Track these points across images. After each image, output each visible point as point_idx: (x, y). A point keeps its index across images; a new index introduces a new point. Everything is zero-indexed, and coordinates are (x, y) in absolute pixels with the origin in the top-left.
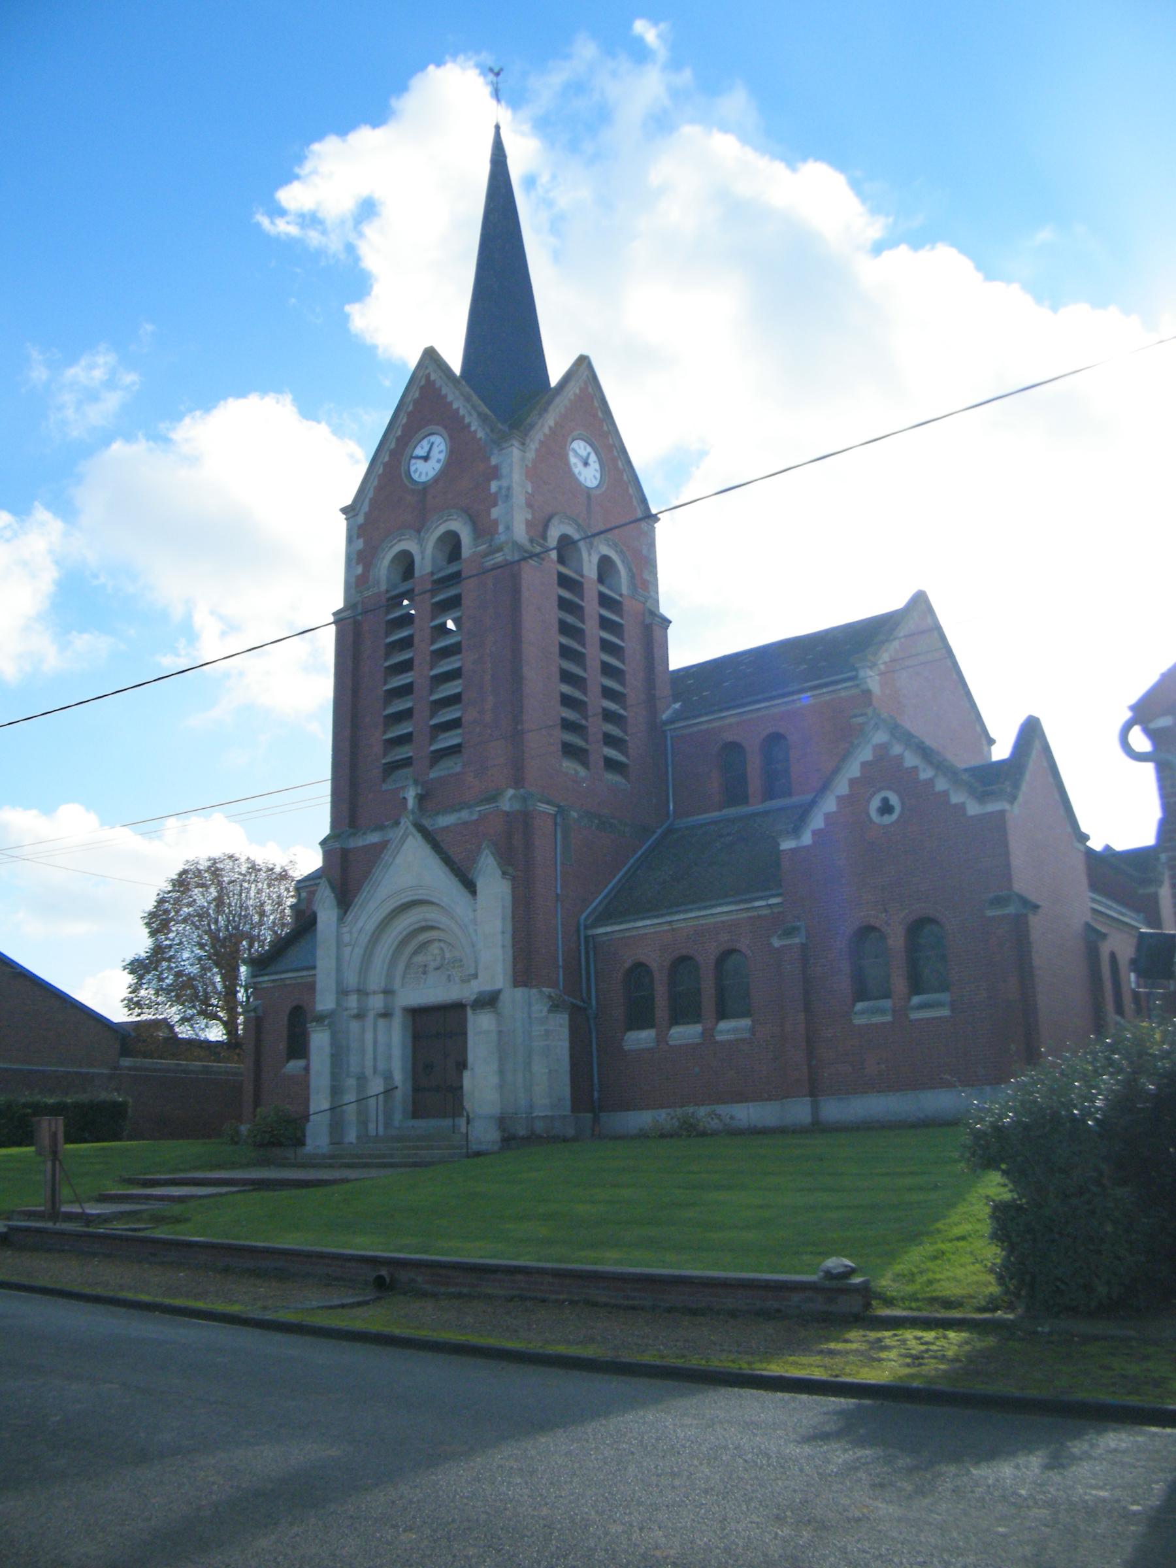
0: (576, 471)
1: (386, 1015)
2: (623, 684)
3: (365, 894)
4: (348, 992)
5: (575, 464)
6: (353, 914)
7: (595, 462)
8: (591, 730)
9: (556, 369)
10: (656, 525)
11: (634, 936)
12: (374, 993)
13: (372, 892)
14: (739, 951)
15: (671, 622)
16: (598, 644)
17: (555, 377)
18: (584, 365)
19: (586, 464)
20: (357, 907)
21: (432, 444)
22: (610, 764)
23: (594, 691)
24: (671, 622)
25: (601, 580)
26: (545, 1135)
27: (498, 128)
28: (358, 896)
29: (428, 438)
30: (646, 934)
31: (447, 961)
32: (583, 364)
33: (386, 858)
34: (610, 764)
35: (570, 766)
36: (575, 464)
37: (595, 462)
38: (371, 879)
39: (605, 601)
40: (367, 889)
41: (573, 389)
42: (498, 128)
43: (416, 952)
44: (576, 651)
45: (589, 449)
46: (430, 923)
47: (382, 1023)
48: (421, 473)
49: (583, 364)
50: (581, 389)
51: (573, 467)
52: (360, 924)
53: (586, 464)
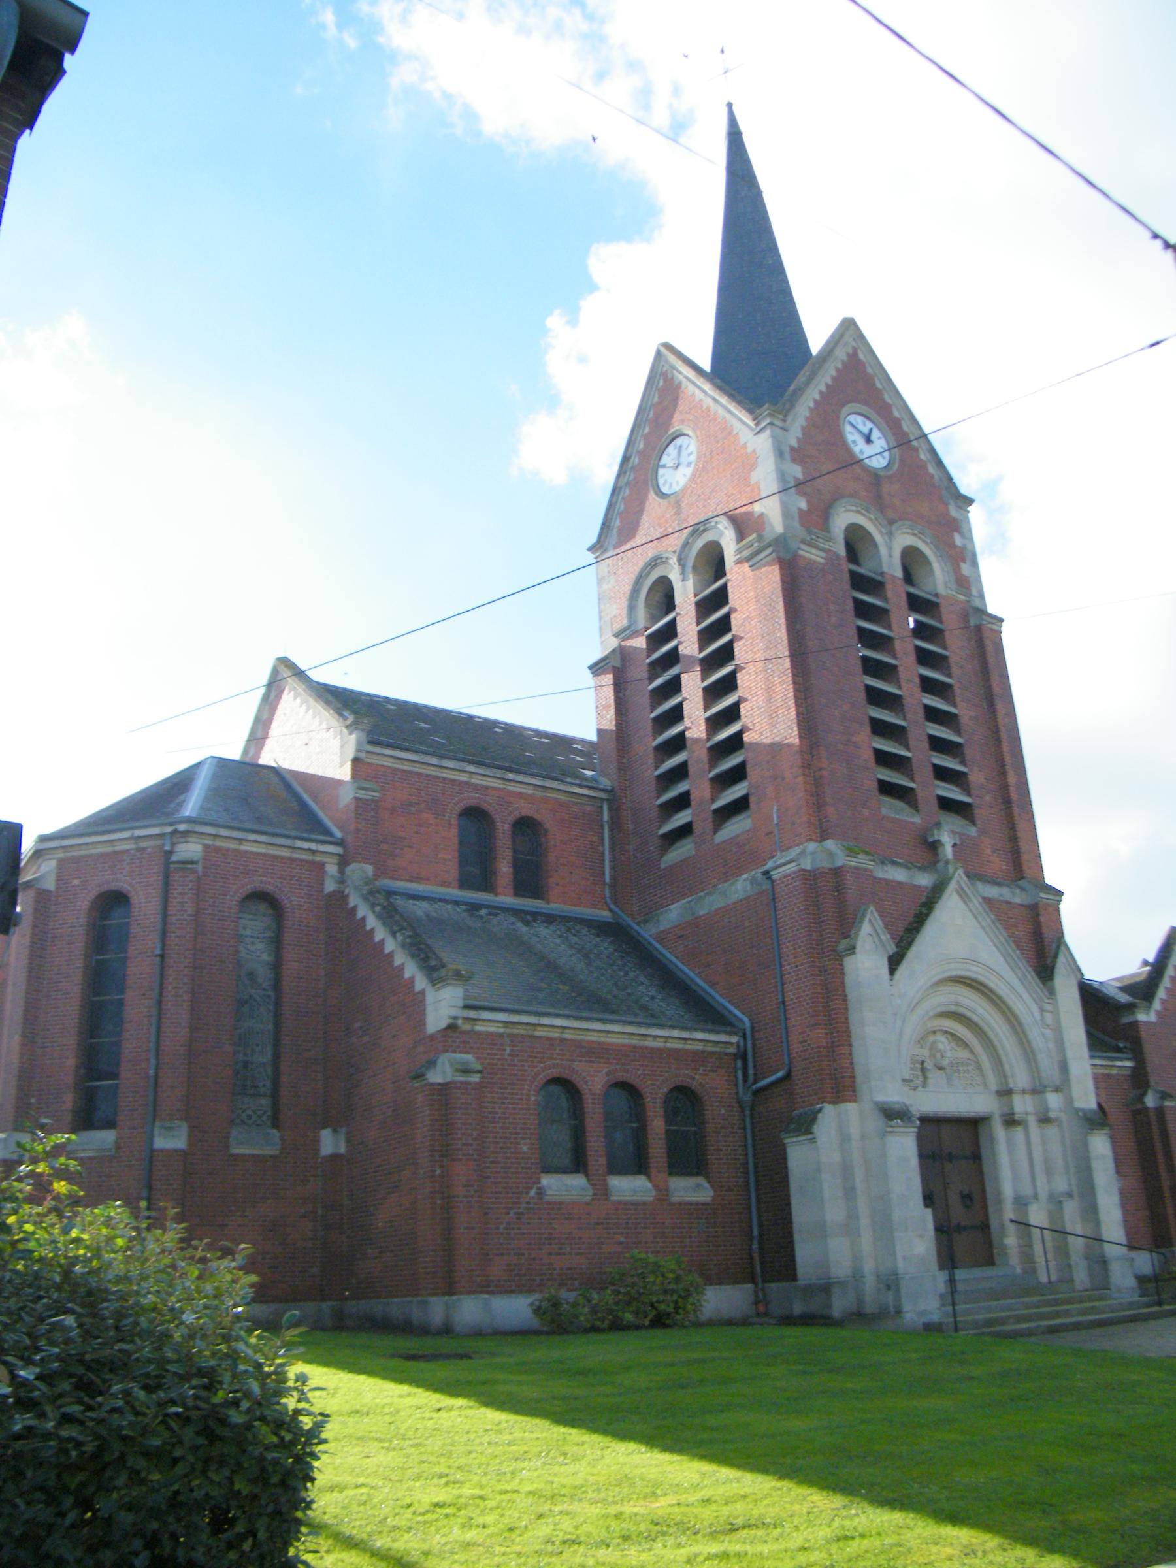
0: (856, 450)
2: (958, 732)
5: (854, 442)
7: (879, 438)
8: (920, 794)
9: (817, 337)
10: (969, 509)
15: (1002, 620)
16: (935, 802)
17: (816, 344)
18: (852, 327)
19: (868, 440)
21: (681, 447)
22: (946, 804)
23: (923, 773)
24: (1002, 620)
25: (908, 578)
27: (730, 105)
29: (673, 443)
32: (849, 327)
34: (946, 804)
35: (891, 808)
36: (854, 442)
37: (879, 438)
39: (916, 604)
41: (841, 354)
42: (730, 105)
44: (882, 635)
45: (869, 425)
48: (671, 485)
49: (849, 327)
50: (848, 354)
51: (852, 445)
53: (868, 440)
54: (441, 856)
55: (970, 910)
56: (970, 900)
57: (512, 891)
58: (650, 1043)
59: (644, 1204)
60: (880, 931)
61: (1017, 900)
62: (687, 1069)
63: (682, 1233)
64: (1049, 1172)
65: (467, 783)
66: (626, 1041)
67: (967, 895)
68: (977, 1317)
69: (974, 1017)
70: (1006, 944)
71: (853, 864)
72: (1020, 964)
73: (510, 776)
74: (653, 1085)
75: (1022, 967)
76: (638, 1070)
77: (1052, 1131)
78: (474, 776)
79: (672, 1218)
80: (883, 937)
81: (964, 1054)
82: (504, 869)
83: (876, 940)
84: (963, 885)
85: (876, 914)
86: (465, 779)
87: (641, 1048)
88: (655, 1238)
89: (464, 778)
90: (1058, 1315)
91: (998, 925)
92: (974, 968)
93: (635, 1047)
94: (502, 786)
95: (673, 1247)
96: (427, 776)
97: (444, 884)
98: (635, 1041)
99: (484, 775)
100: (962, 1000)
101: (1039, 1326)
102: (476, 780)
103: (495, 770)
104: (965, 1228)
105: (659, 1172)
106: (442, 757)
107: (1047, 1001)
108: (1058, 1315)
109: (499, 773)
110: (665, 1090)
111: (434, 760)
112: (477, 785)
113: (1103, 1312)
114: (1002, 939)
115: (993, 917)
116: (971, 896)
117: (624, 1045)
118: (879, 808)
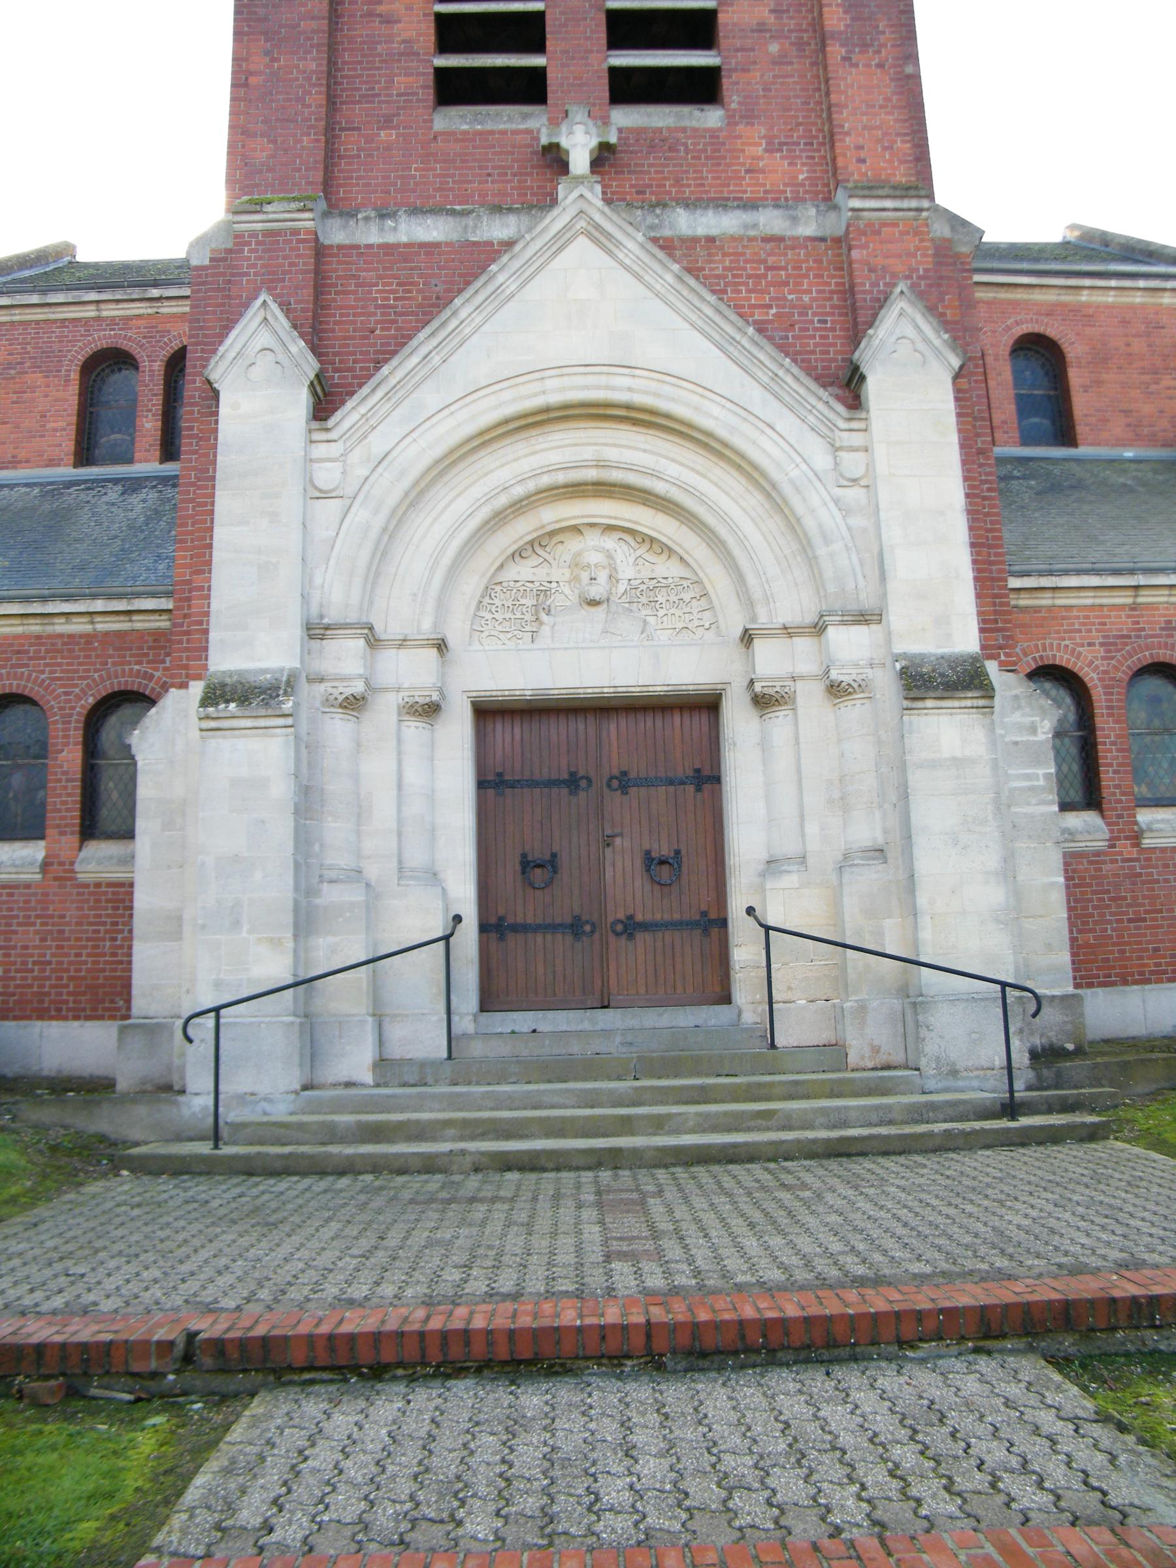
1: (430, 710)
3: (415, 360)
4: (327, 628)
6: (362, 410)
11: (1037, 609)
12: (403, 643)
13: (436, 360)
14: (34, 703)
20: (380, 393)
26: (1070, 1047)
28: (394, 362)
30: (1069, 608)
31: (622, 588)
33: (501, 278)
38: (443, 324)
40: (424, 350)
43: (518, 554)
46: (616, 476)
47: (414, 729)
52: (378, 443)
54: (50, 425)
55: (626, 268)
56: (618, 245)
57: (158, 453)
58: (61, 627)
59: (28, 886)
60: (286, 339)
61: (807, 229)
62: (139, 663)
63: (98, 932)
64: (842, 803)
65: (98, 319)
66: (19, 630)
67: (609, 236)
68: (336, 1118)
69: (660, 487)
70: (717, 319)
71: (259, 226)
72: (761, 356)
73: (155, 292)
74: (66, 694)
75: (767, 362)
76: (43, 672)
77: (854, 711)
78: (103, 306)
79: (79, 909)
80: (294, 349)
81: (667, 569)
82: (148, 425)
83: (281, 357)
84: (598, 217)
85: (274, 307)
86: (93, 314)
87: (50, 636)
88: (43, 940)
89: (90, 312)
90: (626, 1126)
91: (692, 282)
92: (626, 382)
93: (39, 637)
94: (150, 311)
95: (79, 955)
96: (37, 322)
97: (51, 463)
98: (35, 628)
99: (118, 301)
100: (612, 454)
101: (463, 1152)
102: (109, 311)
103: (129, 290)
104: (645, 927)
105: (63, 833)
106: (44, 292)
107: (843, 425)
108: (626, 1126)
109: (136, 293)
110: (91, 700)
111: (35, 299)
112: (113, 318)
113: (810, 1127)
114: (709, 312)
115: (676, 267)
116: (619, 235)
117: (17, 637)
118: (432, 121)
